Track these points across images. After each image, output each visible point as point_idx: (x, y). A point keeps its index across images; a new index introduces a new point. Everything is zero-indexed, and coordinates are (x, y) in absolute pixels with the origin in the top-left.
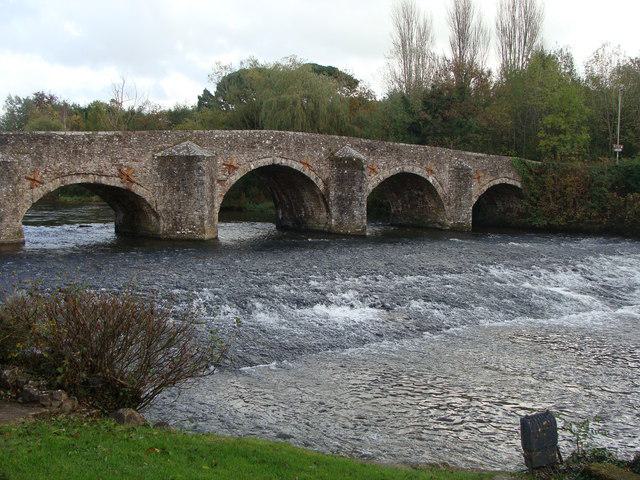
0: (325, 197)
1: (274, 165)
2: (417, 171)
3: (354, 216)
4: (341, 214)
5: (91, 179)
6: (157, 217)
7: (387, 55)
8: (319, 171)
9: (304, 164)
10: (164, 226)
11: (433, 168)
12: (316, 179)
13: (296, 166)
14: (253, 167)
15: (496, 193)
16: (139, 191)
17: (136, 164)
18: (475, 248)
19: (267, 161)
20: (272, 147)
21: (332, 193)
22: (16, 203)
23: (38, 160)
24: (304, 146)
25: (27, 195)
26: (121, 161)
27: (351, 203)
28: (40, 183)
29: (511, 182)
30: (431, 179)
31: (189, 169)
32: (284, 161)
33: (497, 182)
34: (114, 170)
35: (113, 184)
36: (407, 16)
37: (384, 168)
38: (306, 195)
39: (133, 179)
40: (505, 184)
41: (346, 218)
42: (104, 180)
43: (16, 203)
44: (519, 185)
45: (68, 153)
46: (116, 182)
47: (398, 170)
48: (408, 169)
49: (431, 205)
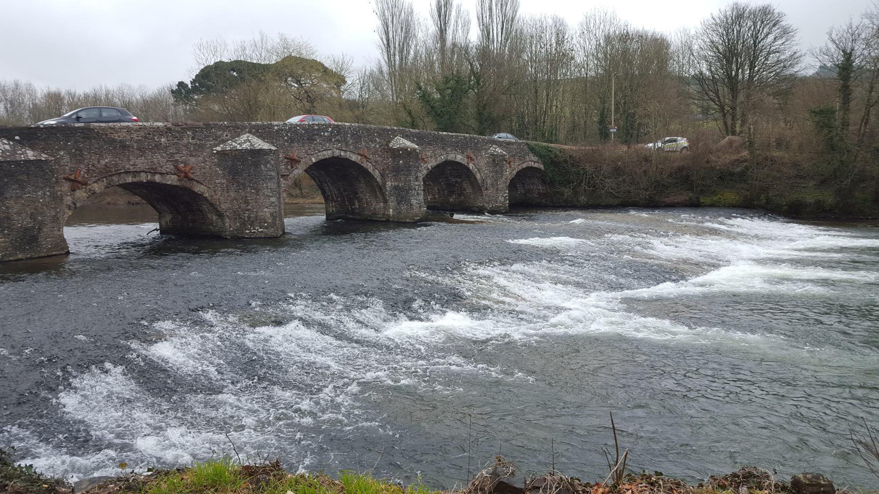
0: (381, 189)
1: (333, 157)
2: (459, 158)
3: (411, 205)
4: (399, 204)
5: (144, 178)
6: (221, 216)
7: (834, 36)
8: (376, 162)
9: (361, 155)
10: (230, 226)
11: (472, 156)
12: (373, 170)
13: (354, 158)
14: (314, 160)
15: (524, 174)
16: (198, 188)
17: (193, 159)
18: (437, 231)
19: (327, 154)
20: (331, 140)
21: (389, 184)
22: (55, 208)
23: (79, 157)
24: (361, 137)
25: (68, 200)
26: (177, 157)
27: (408, 193)
28: (83, 184)
29: (536, 165)
30: (471, 166)
31: (256, 165)
32: (342, 153)
33: (524, 166)
34: (170, 167)
35: (169, 183)
36: (712, 14)
37: (431, 157)
38: (362, 186)
39: (191, 176)
40: (532, 167)
41: (404, 207)
42: (157, 178)
43: (55, 208)
44: (542, 167)
45: (115, 148)
46: (172, 180)
47: (443, 158)
48: (451, 157)
49: (469, 190)
